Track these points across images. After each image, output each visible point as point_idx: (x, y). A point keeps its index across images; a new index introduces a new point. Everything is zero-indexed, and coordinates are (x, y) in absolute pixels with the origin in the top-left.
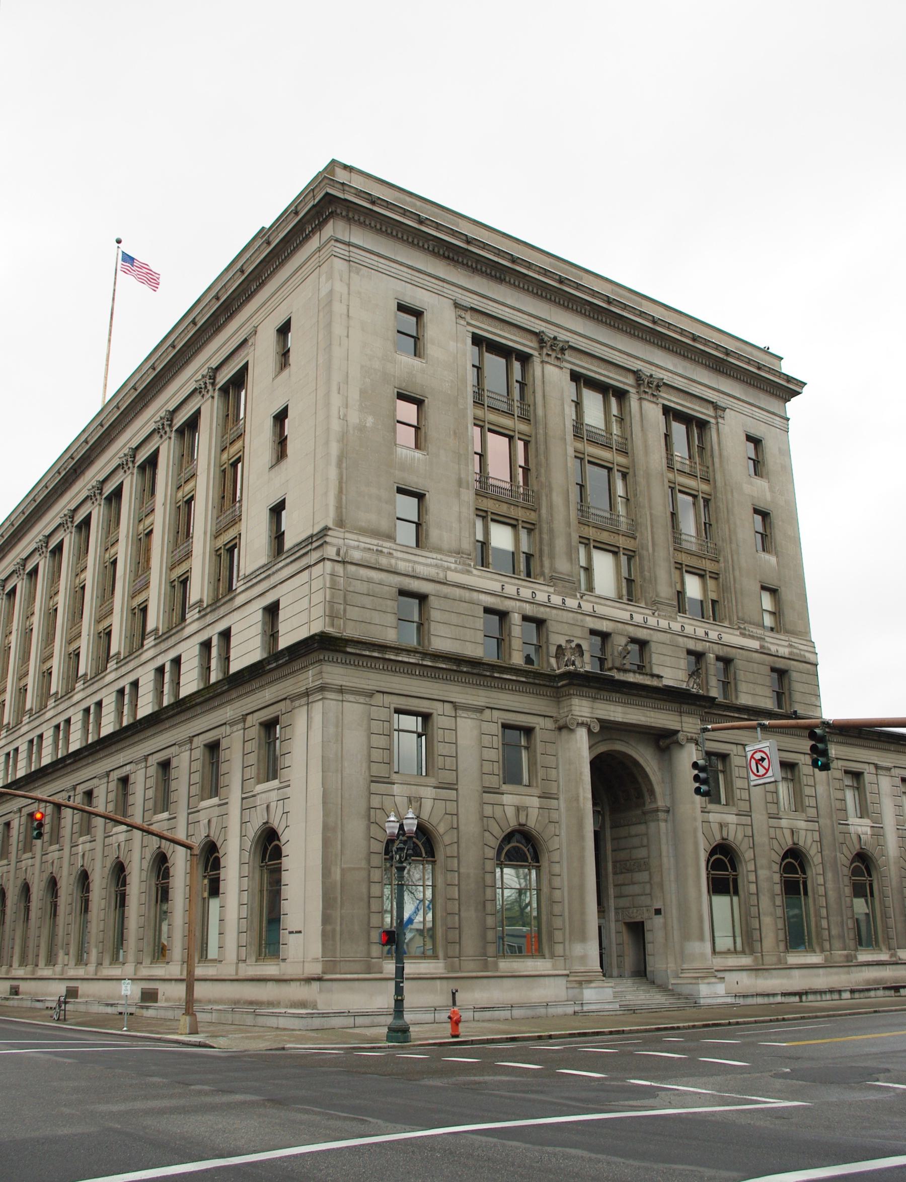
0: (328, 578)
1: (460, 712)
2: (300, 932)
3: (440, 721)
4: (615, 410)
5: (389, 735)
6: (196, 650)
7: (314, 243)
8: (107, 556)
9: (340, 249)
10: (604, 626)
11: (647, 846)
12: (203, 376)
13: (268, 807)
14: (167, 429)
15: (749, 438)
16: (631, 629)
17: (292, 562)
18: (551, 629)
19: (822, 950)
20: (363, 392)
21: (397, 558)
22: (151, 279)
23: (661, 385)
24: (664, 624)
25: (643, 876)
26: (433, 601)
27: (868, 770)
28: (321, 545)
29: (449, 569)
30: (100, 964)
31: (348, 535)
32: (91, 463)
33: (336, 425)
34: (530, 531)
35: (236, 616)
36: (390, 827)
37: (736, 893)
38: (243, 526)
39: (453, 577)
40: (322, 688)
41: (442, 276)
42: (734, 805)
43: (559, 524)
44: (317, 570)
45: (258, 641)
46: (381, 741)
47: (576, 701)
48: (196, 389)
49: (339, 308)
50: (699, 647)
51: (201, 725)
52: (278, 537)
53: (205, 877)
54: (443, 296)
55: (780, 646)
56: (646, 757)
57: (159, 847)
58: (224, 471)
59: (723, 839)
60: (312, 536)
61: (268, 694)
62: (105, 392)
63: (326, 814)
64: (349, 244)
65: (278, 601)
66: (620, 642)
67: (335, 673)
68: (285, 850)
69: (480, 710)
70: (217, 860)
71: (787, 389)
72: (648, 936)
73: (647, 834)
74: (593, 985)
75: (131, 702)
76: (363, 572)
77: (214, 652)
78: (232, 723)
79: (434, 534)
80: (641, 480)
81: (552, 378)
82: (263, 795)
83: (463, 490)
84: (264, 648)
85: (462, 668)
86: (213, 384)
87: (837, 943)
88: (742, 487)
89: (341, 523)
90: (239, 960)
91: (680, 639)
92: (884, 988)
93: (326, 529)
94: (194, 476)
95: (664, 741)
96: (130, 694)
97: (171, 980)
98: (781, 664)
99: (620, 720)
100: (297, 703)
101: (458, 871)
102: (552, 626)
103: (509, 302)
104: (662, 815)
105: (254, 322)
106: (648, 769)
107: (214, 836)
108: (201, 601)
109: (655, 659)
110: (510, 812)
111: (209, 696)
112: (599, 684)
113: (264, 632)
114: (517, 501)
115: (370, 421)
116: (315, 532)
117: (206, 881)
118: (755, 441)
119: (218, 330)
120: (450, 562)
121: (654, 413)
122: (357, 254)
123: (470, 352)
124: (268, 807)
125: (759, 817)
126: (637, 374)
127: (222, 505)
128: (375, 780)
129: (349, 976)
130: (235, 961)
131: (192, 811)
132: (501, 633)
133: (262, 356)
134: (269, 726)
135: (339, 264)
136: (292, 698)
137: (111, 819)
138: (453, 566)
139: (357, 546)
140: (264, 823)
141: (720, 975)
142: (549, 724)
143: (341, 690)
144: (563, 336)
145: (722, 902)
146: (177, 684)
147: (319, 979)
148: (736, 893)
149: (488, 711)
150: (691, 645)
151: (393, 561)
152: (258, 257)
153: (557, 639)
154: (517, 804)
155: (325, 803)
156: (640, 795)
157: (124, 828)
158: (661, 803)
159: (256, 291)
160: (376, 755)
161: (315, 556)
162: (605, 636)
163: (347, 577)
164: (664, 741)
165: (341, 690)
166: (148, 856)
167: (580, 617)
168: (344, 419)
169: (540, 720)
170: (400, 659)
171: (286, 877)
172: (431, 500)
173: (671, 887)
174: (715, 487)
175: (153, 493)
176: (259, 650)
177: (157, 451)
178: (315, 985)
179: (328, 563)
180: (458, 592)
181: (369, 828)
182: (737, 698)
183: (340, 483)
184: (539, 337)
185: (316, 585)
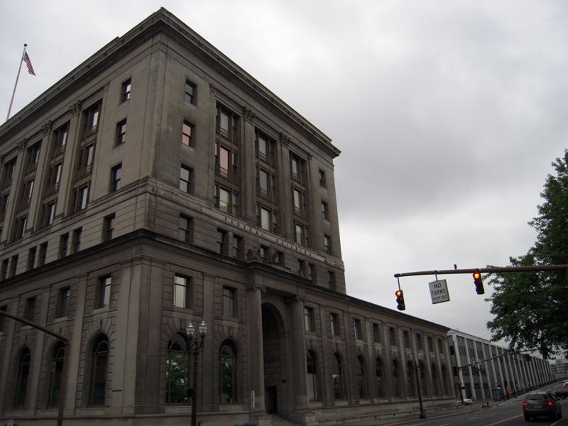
0: (147, 202)
1: (205, 278)
2: (120, 391)
3: (197, 281)
7: (149, 43)
8: (26, 179)
9: (163, 48)
10: (267, 244)
12: (46, 124)
13: (101, 322)
14: (49, 130)
15: (189, 82)
16: (277, 247)
17: (126, 193)
19: (347, 400)
20: (169, 115)
21: (180, 198)
24: (289, 246)
28: (145, 185)
30: (37, 408)
33: (155, 128)
35: (86, 221)
36: (189, 331)
37: (315, 372)
38: (93, 177)
39: (204, 210)
40: (142, 258)
41: (205, 71)
43: (249, 194)
44: (141, 198)
45: (100, 234)
46: (219, 300)
48: (69, 111)
49: (160, 74)
50: (302, 258)
51: (60, 278)
52: (114, 182)
53: (53, 361)
56: (280, 306)
57: (25, 344)
59: (230, 336)
60: (139, 181)
61: (105, 261)
62: (10, 111)
63: (140, 325)
64: (167, 46)
65: (47, 242)
66: (273, 252)
67: (148, 251)
68: (111, 345)
71: (334, 153)
74: (263, 417)
75: (12, 266)
78: (80, 277)
79: (197, 189)
80: (281, 180)
81: (249, 128)
82: (99, 315)
83: (210, 171)
85: (208, 256)
86: (80, 109)
89: (155, 175)
90: (76, 407)
91: (295, 253)
92: (337, 420)
94: (10, 185)
95: (289, 299)
96: (12, 262)
97: (26, 419)
98: (332, 269)
99: (274, 287)
102: (246, 241)
104: (287, 335)
105: (108, 79)
108: (63, 214)
109: (286, 261)
111: (64, 262)
112: (266, 269)
113: (104, 229)
114: (233, 182)
115: (171, 129)
116: (141, 178)
117: (54, 363)
120: (204, 203)
124: (101, 322)
125: (324, 337)
126: (280, 134)
129: (148, 415)
132: (223, 240)
133: (111, 97)
134: (64, 290)
135: (162, 54)
136: (121, 263)
137: (20, 321)
139: (162, 188)
140: (98, 331)
141: (313, 411)
142: (243, 287)
143: (151, 260)
147: (134, 418)
148: (315, 372)
149: (217, 278)
150: (300, 257)
154: (230, 325)
155: (139, 319)
157: (29, 327)
158: (286, 328)
159: (112, 65)
160: (166, 296)
161: (141, 190)
163: (156, 202)
164: (289, 299)
165: (151, 260)
166: (16, 349)
168: (160, 125)
170: (181, 247)
172: (197, 172)
176: (100, 239)
177: (41, 141)
179: (148, 195)
182: (316, 282)
183: (156, 156)
184: (244, 109)
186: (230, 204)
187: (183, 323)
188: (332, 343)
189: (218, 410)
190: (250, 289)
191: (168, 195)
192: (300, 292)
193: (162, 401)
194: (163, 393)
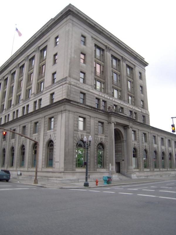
0: (67, 87)
1: (70, 112)
3: (88, 119)
4: (102, 53)
5: (78, 121)
6: (22, 109)
7: (65, 20)
9: (71, 21)
10: (116, 104)
11: (121, 148)
15: (83, 36)
18: (107, 103)
19: (149, 168)
21: (80, 85)
22: (20, 34)
23: (126, 60)
25: (120, 153)
26: (87, 95)
27: (157, 136)
29: (89, 89)
30: (28, 167)
31: (71, 79)
32: (8, 67)
33: (69, 56)
34: (103, 84)
37: (136, 157)
38: (45, 78)
39: (90, 90)
40: (65, 110)
42: (136, 140)
43: (109, 83)
47: (112, 118)
51: (34, 118)
52: (53, 80)
54: (89, 34)
55: (144, 111)
56: (122, 130)
58: (19, 82)
66: (119, 107)
67: (68, 107)
68: (54, 145)
69: (95, 118)
70: (36, 147)
71: (146, 64)
72: (121, 165)
73: (121, 145)
75: (16, 114)
76: (74, 87)
77: (37, 103)
78: (42, 118)
79: (87, 81)
82: (49, 133)
84: (50, 102)
85: (92, 109)
87: (152, 167)
88: (139, 82)
89: (70, 76)
90: (42, 168)
93: (67, 77)
95: (126, 127)
96: (16, 112)
98: (144, 115)
100: (58, 113)
101: (90, 151)
102: (108, 103)
103: (119, 51)
104: (124, 142)
106: (122, 131)
107: (24, 144)
110: (100, 139)
112: (116, 114)
113: (50, 99)
114: (102, 78)
116: (64, 78)
118: (140, 73)
119: (40, 39)
120: (90, 87)
121: (125, 65)
122: (74, 23)
123: (94, 48)
124: (50, 136)
125: (140, 143)
126: (122, 57)
127: (28, 81)
128: (75, 130)
130: (41, 168)
131: (10, 141)
132: (98, 103)
133: (51, 44)
134: (36, 123)
135: (71, 24)
136: (57, 112)
138: (90, 88)
139: (73, 81)
141: (135, 173)
142: (107, 122)
143: (69, 111)
144: (110, 47)
145: (134, 158)
146: (8, 119)
147: (64, 172)
148: (136, 157)
151: (79, 86)
152: (59, 16)
153: (108, 105)
154: (101, 137)
156: (120, 138)
158: (125, 139)
162: (116, 106)
163: (70, 87)
164: (126, 127)
167: (112, 101)
168: (71, 55)
169: (105, 121)
171: (55, 150)
173: (126, 156)
174: (105, 64)
175: (6, 84)
178: (62, 174)
179: (67, 84)
180: (91, 93)
181: (73, 140)
184: (106, 46)
185: (64, 89)
186: (101, 88)
187: (102, 140)
188: (143, 145)
189: (96, 171)
190: (109, 123)
191: (75, 84)
192: (130, 124)
193: (74, 166)
194: (75, 163)
